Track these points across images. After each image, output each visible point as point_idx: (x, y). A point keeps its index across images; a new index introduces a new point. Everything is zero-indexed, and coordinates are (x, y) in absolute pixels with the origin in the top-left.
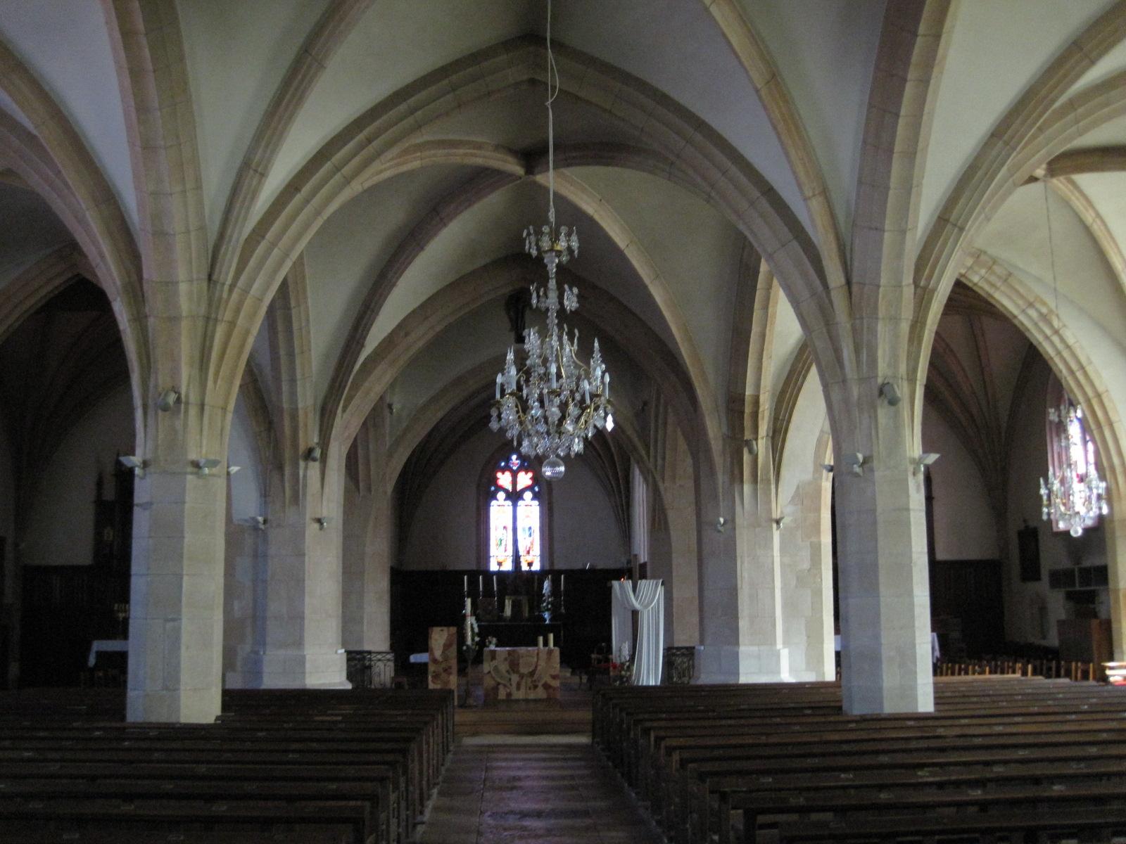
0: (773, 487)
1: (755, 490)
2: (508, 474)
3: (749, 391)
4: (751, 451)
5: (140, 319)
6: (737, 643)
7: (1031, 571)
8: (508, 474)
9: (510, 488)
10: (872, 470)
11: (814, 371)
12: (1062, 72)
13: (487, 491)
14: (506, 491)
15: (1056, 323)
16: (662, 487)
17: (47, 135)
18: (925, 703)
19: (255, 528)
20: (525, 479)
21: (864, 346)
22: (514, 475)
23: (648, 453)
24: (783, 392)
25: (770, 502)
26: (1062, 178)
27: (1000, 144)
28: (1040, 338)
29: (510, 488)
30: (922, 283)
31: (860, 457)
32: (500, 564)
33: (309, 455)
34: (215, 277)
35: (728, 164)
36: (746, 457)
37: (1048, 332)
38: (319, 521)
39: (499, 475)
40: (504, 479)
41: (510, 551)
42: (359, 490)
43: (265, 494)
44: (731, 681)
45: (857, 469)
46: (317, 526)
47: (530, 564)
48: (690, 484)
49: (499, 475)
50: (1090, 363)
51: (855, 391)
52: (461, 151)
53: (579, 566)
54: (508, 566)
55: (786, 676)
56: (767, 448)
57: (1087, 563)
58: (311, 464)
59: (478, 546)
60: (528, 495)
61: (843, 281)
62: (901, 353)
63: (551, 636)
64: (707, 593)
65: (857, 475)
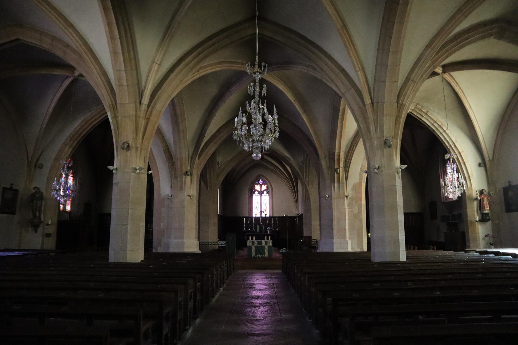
0: (345, 184)
1: (339, 186)
3: (336, 152)
4: (337, 173)
5: (115, 117)
6: (333, 238)
7: (434, 216)
10: (382, 171)
11: (361, 140)
12: (450, 25)
13: (252, 191)
15: (445, 129)
16: (307, 187)
17: (82, 50)
18: (403, 258)
19: (168, 199)
20: (264, 187)
21: (379, 125)
22: (261, 186)
23: (303, 176)
24: (348, 152)
25: (344, 190)
26: (447, 74)
27: (430, 50)
28: (439, 133)
29: (259, 190)
30: (400, 102)
31: (377, 166)
32: (256, 215)
33: (186, 174)
34: (142, 102)
35: (328, 61)
36: (336, 175)
38: (189, 196)
39: (256, 186)
40: (257, 187)
42: (207, 186)
44: (331, 251)
45: (376, 170)
46: (189, 198)
47: (266, 215)
48: (317, 187)
49: (256, 186)
51: (376, 143)
52: (235, 65)
53: (282, 216)
54: (258, 215)
55: (350, 250)
56: (343, 174)
57: (455, 213)
58: (187, 176)
59: (138, 77)
60: (265, 192)
61: (370, 102)
62: (393, 130)
63: (270, 237)
64: (322, 221)
65: (376, 173)
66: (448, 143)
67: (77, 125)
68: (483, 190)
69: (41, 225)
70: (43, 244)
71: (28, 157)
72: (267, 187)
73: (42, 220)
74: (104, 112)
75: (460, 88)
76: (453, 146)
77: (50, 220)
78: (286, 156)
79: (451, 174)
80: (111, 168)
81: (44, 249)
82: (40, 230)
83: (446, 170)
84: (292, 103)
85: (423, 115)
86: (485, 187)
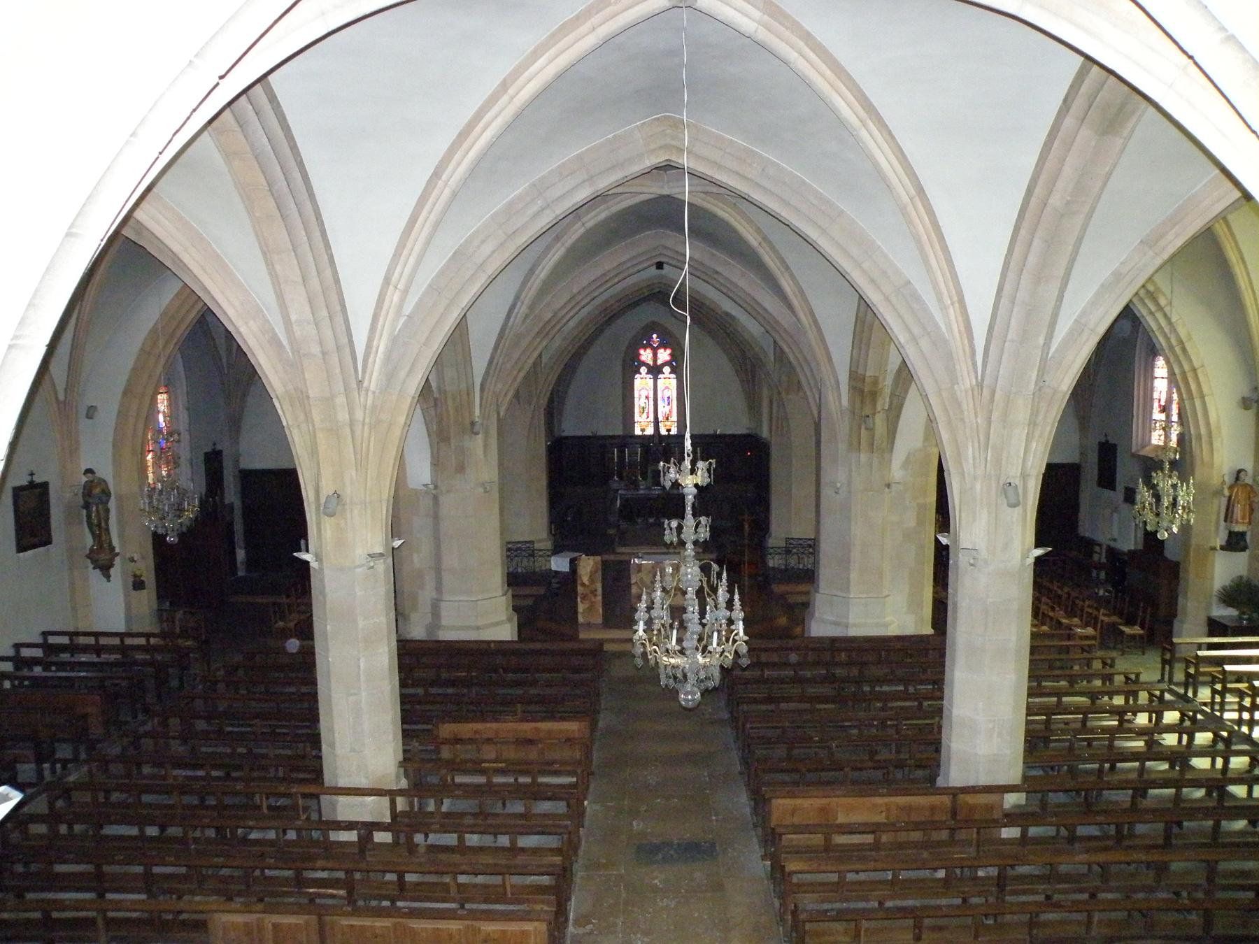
2: (649, 351)
6: (848, 590)
8: (649, 351)
9: (651, 363)
13: (631, 366)
14: (647, 365)
15: (1163, 302)
20: (664, 355)
28: (1144, 312)
29: (651, 363)
32: (643, 430)
37: (1153, 309)
39: (642, 352)
40: (646, 355)
41: (652, 418)
43: (436, 463)
47: (669, 430)
49: (642, 352)
50: (1190, 339)
53: (712, 432)
54: (650, 431)
59: (600, 331)
60: (667, 369)
68: (1239, 472)
69: (117, 560)
71: (56, 393)
72: (671, 355)
73: (117, 550)
76: (1178, 349)
77: (132, 542)
78: (727, 314)
83: (1153, 367)
86: (1249, 466)
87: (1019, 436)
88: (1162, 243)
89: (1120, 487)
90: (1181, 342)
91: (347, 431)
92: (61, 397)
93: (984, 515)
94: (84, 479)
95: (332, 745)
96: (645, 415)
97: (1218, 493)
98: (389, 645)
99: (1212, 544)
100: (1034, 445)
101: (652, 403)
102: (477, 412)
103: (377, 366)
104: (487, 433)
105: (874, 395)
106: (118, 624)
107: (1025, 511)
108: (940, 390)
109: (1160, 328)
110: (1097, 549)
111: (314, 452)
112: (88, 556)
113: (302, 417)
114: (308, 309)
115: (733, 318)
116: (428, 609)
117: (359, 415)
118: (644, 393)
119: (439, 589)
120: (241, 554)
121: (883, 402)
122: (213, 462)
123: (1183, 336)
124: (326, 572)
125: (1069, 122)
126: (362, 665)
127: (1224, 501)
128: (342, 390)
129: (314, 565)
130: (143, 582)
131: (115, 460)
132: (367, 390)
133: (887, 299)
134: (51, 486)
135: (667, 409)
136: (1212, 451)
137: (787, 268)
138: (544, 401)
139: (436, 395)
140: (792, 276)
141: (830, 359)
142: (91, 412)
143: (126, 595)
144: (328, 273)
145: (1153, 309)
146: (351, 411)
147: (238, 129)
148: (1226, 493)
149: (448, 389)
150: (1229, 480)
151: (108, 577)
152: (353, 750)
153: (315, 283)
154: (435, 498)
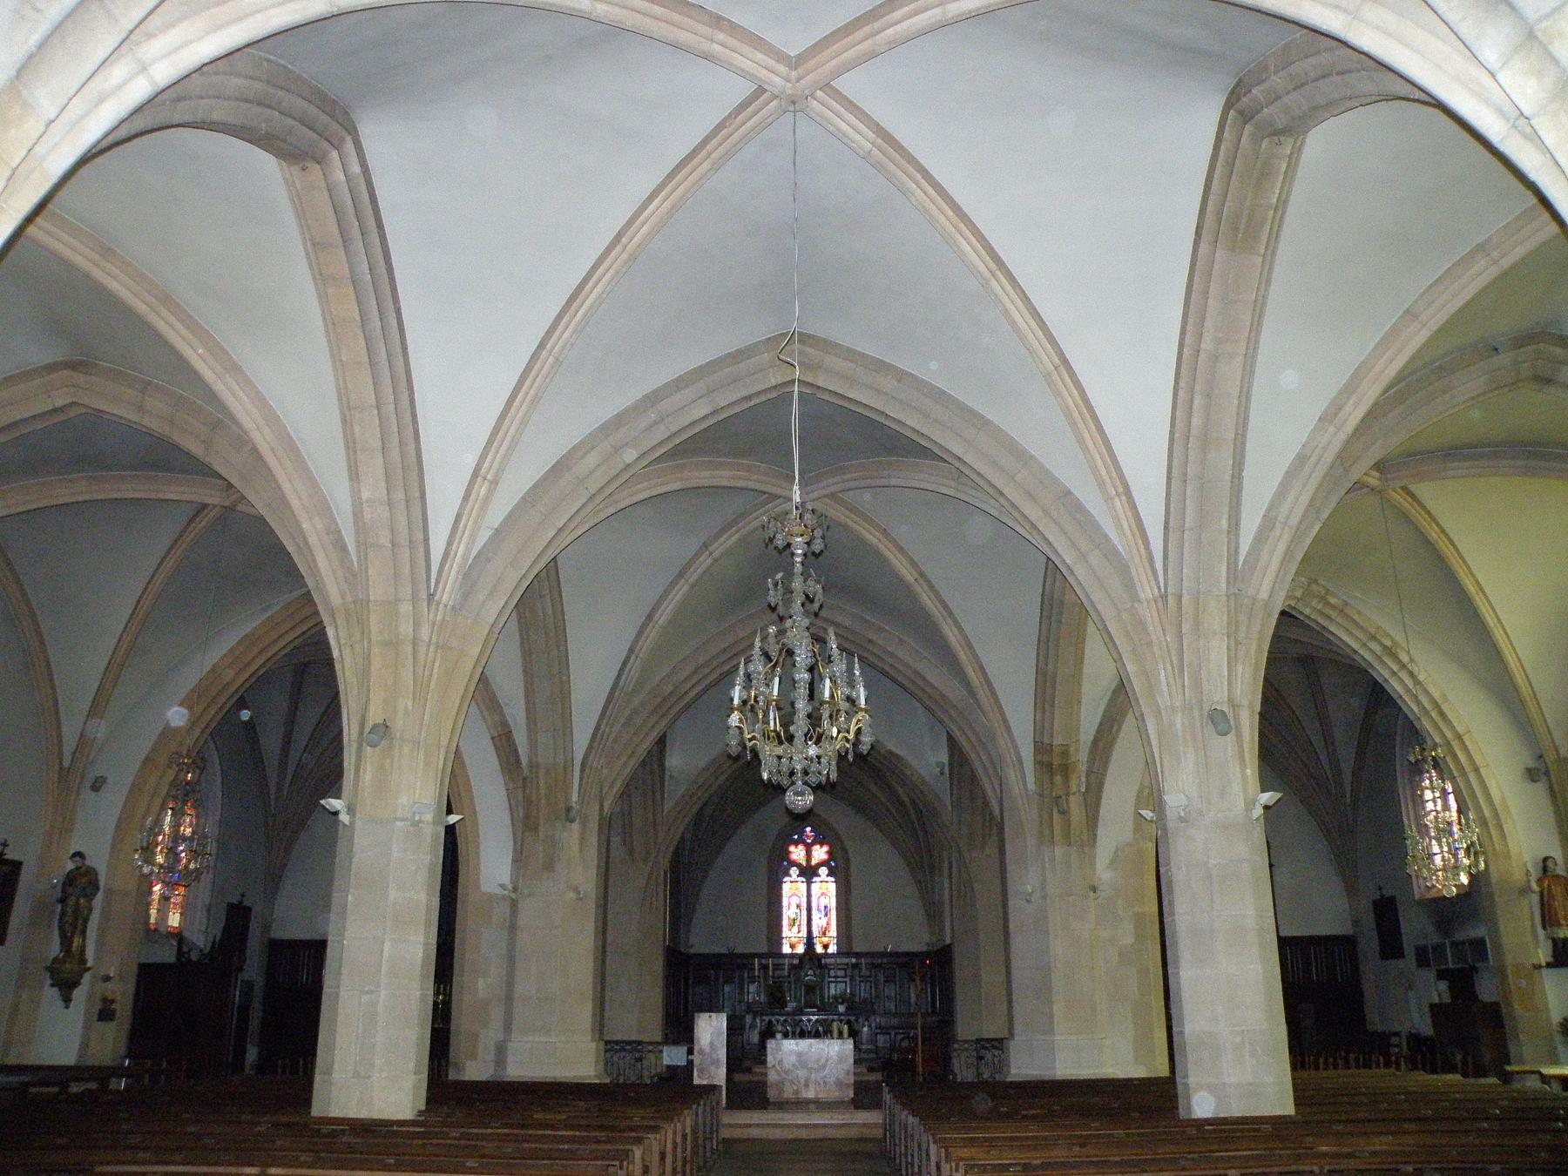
2: (801, 847)
4: (1063, 812)
6: (1051, 1031)
7: (1391, 946)
13: (778, 866)
14: (798, 865)
20: (820, 853)
37: (1395, 668)
39: (792, 848)
40: (798, 853)
43: (519, 859)
47: (826, 947)
49: (792, 848)
50: (1446, 700)
57: (1461, 936)
60: (823, 871)
66: (1419, 703)
67: (222, 648)
68: (1545, 860)
69: (87, 977)
70: (84, 1046)
71: (61, 754)
72: (829, 853)
73: (89, 964)
74: (307, 611)
75: (1443, 531)
77: (110, 961)
78: (891, 752)
79: (1435, 801)
80: (334, 804)
81: (90, 1062)
82: (79, 994)
84: (908, 587)
85: (1333, 614)
86: (1556, 852)
87: (1217, 653)
88: (1341, 416)
89: (1409, 950)
90: (1437, 706)
91: (409, 649)
92: (66, 763)
93: (1190, 751)
94: (70, 866)
95: (329, 1071)
96: (795, 929)
97: (1525, 890)
98: (427, 934)
99: (1535, 961)
100: (1240, 669)
101: (804, 913)
102: (575, 798)
103: (453, 573)
104: (584, 826)
105: (1066, 770)
106: (66, 1055)
107: (1239, 736)
108: (1119, 612)
109: (1409, 690)
110: (1395, 1040)
111: (365, 673)
112: (47, 968)
113: (358, 635)
114: (383, 485)
115: (898, 757)
116: (491, 1056)
117: (425, 632)
118: (795, 901)
119: (507, 1027)
120: (252, 1054)
121: (1078, 782)
122: (237, 917)
123: (1436, 695)
124: (358, 825)
125: (1204, 247)
126: (386, 954)
127: (1535, 899)
128: (409, 597)
129: (344, 818)
130: (114, 1011)
131: (113, 847)
132: (438, 603)
133: (1046, 512)
134: (25, 877)
135: (824, 922)
136: (1503, 837)
137: (951, 614)
138: (665, 862)
139: (526, 772)
140: (956, 623)
141: (1008, 728)
142: (97, 785)
143: (87, 1027)
144: (411, 448)
145: (1395, 668)
146: (416, 625)
147: (340, 243)
148: (1535, 887)
149: (541, 760)
150: (1535, 874)
151: (67, 1000)
152: (357, 1075)
153: (395, 454)
154: (514, 904)
